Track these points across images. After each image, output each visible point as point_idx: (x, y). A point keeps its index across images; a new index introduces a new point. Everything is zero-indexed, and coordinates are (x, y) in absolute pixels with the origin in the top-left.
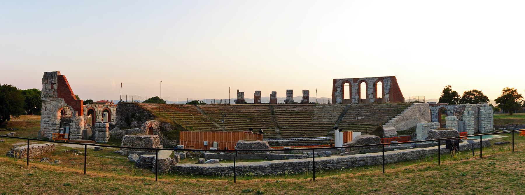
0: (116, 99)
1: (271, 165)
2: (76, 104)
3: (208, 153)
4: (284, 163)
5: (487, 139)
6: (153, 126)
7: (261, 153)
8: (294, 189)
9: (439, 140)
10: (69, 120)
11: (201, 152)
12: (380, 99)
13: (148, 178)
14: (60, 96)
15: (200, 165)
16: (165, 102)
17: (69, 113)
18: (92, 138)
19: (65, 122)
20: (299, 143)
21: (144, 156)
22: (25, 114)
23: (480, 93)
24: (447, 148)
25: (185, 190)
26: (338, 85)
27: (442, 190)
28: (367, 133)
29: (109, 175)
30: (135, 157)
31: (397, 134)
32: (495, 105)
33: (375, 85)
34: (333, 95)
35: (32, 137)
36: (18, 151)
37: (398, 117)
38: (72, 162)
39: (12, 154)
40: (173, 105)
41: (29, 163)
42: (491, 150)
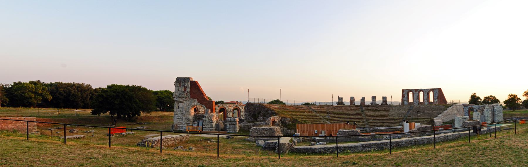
0: (245, 101)
1: (362, 145)
2: (209, 104)
3: (318, 138)
4: (371, 144)
5: (499, 126)
6: (276, 120)
7: (355, 137)
8: (378, 160)
9: (469, 128)
10: (202, 116)
11: (313, 138)
12: (431, 102)
13: (273, 157)
14: (193, 97)
15: (312, 147)
16: (285, 104)
17: (202, 111)
18: (224, 130)
19: (198, 117)
20: (380, 131)
21: (269, 141)
22: (157, 111)
23: (494, 97)
24: (474, 132)
25: (301, 164)
26: (405, 93)
27: (471, 158)
28: (424, 124)
29: (240, 156)
30: (261, 142)
32: (504, 105)
33: (428, 94)
34: (402, 100)
35: (165, 130)
36: (150, 142)
37: (443, 114)
38: (206, 148)
39: (143, 144)
40: (291, 106)
41: (163, 151)
42: (501, 133)
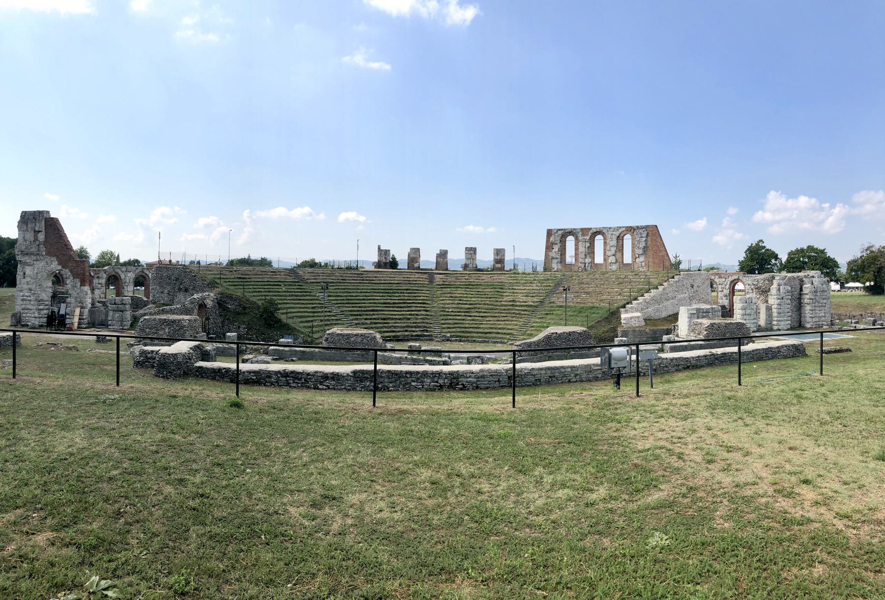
1: (355, 372)
14: (49, 254)
26: (556, 239)
31: (643, 323)
33: (620, 239)
34: (546, 255)
